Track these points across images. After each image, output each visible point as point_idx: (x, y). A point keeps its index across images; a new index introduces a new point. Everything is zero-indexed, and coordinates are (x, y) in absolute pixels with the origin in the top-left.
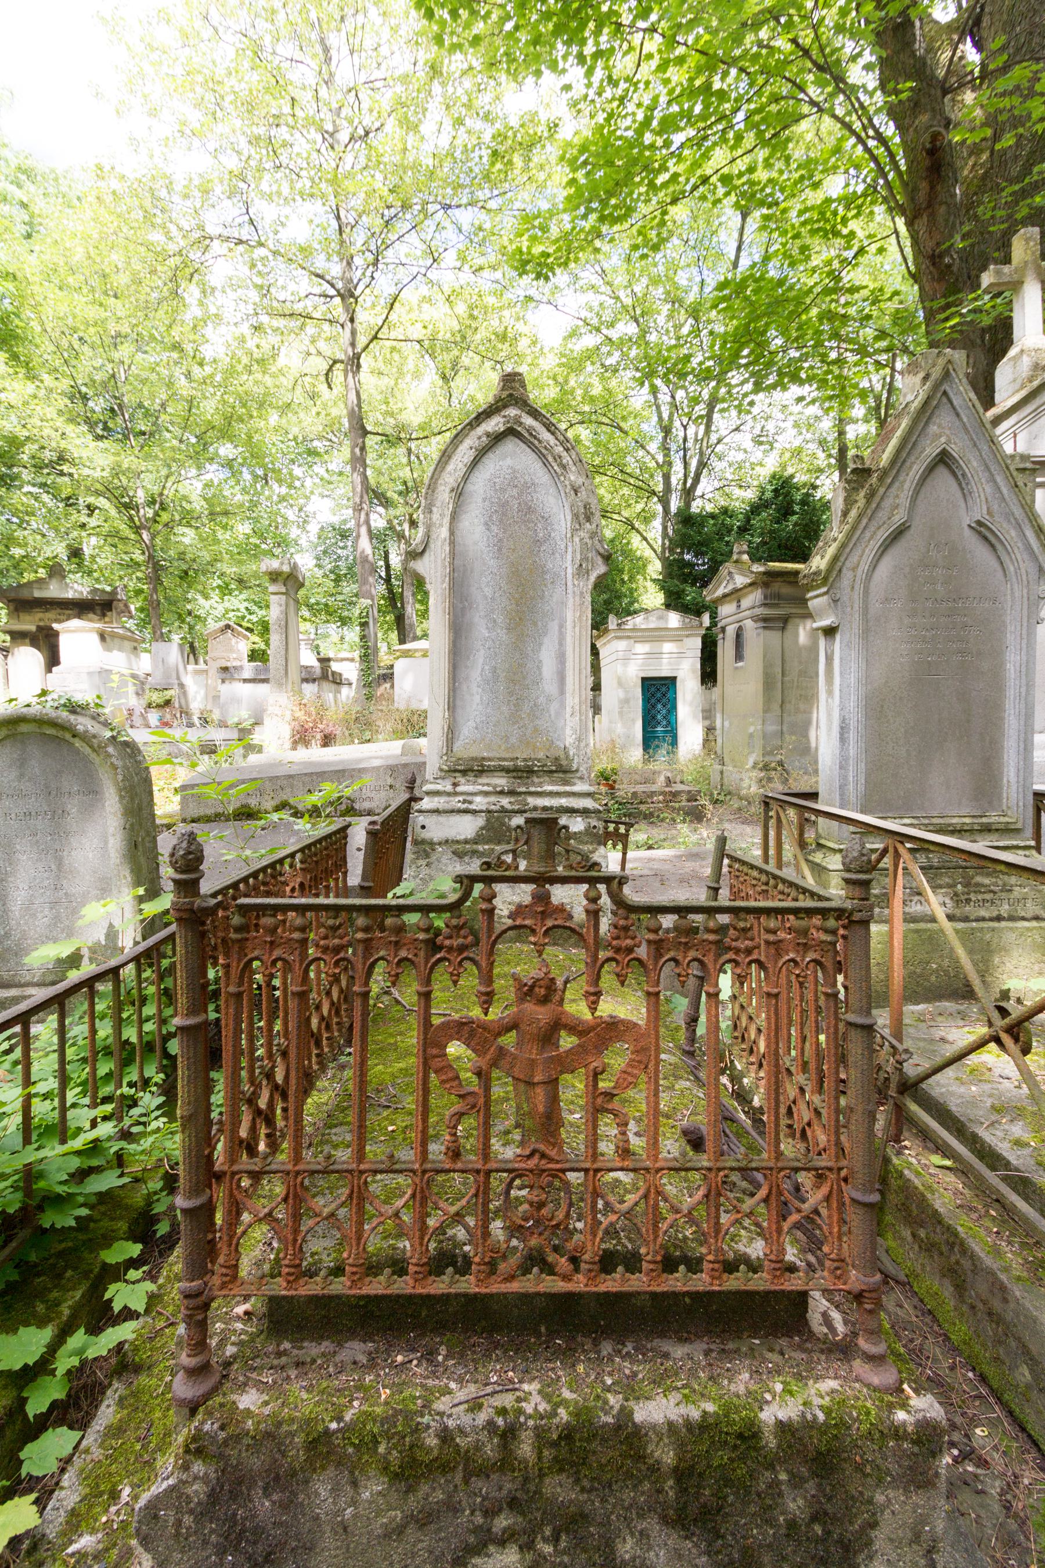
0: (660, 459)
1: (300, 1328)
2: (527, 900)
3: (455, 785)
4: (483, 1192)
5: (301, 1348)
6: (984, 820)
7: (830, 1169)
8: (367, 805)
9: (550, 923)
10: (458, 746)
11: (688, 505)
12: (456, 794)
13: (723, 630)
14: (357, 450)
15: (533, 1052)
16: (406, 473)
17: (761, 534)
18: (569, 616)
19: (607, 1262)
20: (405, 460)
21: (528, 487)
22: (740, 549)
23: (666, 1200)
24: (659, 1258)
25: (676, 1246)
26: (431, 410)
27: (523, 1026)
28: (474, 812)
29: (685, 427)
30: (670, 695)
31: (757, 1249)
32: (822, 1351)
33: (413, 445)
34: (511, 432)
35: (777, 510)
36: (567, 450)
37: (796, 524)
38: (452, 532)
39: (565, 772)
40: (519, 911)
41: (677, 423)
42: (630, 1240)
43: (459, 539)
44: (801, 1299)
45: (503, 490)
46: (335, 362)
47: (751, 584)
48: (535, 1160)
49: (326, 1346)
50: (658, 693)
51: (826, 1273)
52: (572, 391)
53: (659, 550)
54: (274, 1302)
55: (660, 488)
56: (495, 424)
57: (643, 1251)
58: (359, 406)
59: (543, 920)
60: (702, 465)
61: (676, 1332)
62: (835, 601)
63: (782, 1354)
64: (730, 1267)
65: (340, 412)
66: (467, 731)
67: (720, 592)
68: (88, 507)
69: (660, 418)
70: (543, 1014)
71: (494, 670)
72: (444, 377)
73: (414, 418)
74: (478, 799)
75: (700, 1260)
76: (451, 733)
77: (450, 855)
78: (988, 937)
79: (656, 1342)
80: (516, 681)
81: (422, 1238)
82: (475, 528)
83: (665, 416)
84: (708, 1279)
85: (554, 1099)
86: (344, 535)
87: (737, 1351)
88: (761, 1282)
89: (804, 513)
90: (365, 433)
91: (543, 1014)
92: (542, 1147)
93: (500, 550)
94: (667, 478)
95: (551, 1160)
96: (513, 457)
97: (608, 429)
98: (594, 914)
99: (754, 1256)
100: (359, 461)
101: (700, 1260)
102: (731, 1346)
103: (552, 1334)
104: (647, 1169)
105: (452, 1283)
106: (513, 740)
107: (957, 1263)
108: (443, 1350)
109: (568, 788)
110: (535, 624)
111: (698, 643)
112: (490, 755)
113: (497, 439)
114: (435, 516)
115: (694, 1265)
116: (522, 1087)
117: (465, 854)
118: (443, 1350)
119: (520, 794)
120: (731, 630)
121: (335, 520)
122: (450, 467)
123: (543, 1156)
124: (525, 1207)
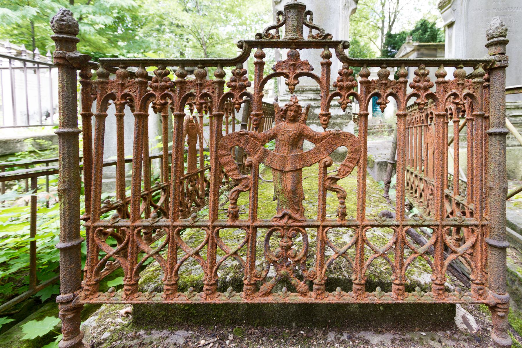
1: (151, 322)
2: (285, 58)
4: (251, 240)
5: (150, 334)
6: (516, 104)
7: (476, 226)
9: (298, 71)
15: (285, 152)
19: (330, 285)
23: (369, 245)
24: (363, 282)
25: (375, 276)
27: (280, 136)
31: (426, 278)
32: (465, 340)
35: (422, 31)
37: (428, 35)
40: (280, 64)
42: (348, 272)
44: (451, 309)
47: (413, 50)
48: (285, 220)
49: (165, 332)
51: (472, 292)
53: (380, 48)
54: (137, 307)
57: (353, 277)
59: (294, 70)
61: (374, 327)
62: (454, 10)
63: (440, 342)
64: (410, 289)
68: (187, 39)
70: (292, 128)
75: (390, 284)
78: (517, 153)
79: (362, 333)
81: (212, 268)
84: (395, 296)
85: (298, 182)
87: (412, 340)
88: (429, 298)
89: (431, 31)
91: (292, 128)
92: (289, 212)
95: (295, 220)
98: (327, 66)
99: (423, 283)
101: (390, 284)
102: (408, 336)
103: (300, 327)
104: (357, 226)
105: (230, 297)
107: (517, 289)
108: (231, 337)
112: (307, 85)
115: (386, 287)
116: (278, 174)
118: (231, 337)
123: (290, 217)
124: (279, 249)
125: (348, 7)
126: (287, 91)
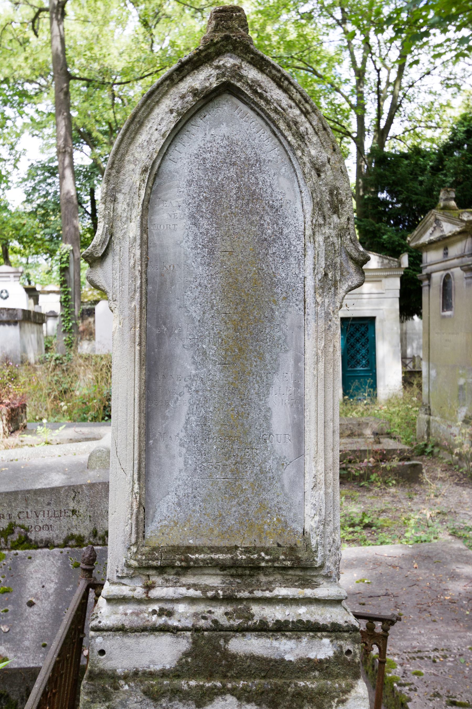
0: (354, 100)
3: (149, 587)
8: (44, 535)
10: (152, 530)
11: (382, 145)
12: (150, 601)
13: (429, 277)
14: (62, 96)
16: (109, 115)
17: (455, 174)
18: (311, 346)
20: (109, 102)
21: (253, 164)
22: (447, 197)
26: (135, 56)
28: (174, 631)
29: (378, 71)
30: (369, 335)
33: (116, 88)
34: (227, 89)
36: (306, 113)
38: (144, 229)
39: (305, 569)
41: (370, 66)
43: (154, 238)
45: (216, 169)
46: (41, 10)
47: (460, 233)
50: (358, 334)
52: (268, 37)
55: (354, 128)
56: (204, 78)
58: (64, 50)
60: (395, 108)
65: (46, 57)
66: (165, 508)
67: (426, 238)
69: (354, 63)
71: (204, 421)
72: (145, 24)
73: (118, 64)
74: (181, 608)
76: (143, 511)
77: (140, 696)
80: (235, 439)
82: (176, 222)
83: (359, 60)
86: (53, 172)
90: (70, 77)
93: (211, 252)
94: (361, 120)
96: (230, 124)
97: (303, 73)
100: (63, 103)
106: (231, 521)
109: (308, 592)
110: (261, 357)
111: (396, 283)
113: (206, 99)
114: (121, 207)
117: (163, 695)
119: (241, 600)
120: (437, 278)
121: (44, 158)
122: (142, 138)
125: (335, 285)
126: (128, 566)
